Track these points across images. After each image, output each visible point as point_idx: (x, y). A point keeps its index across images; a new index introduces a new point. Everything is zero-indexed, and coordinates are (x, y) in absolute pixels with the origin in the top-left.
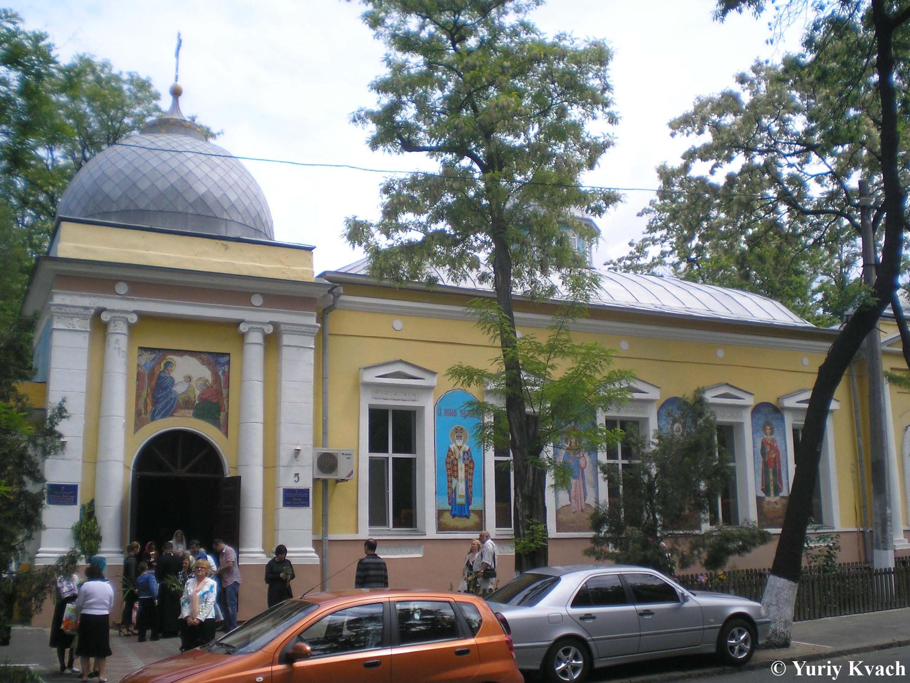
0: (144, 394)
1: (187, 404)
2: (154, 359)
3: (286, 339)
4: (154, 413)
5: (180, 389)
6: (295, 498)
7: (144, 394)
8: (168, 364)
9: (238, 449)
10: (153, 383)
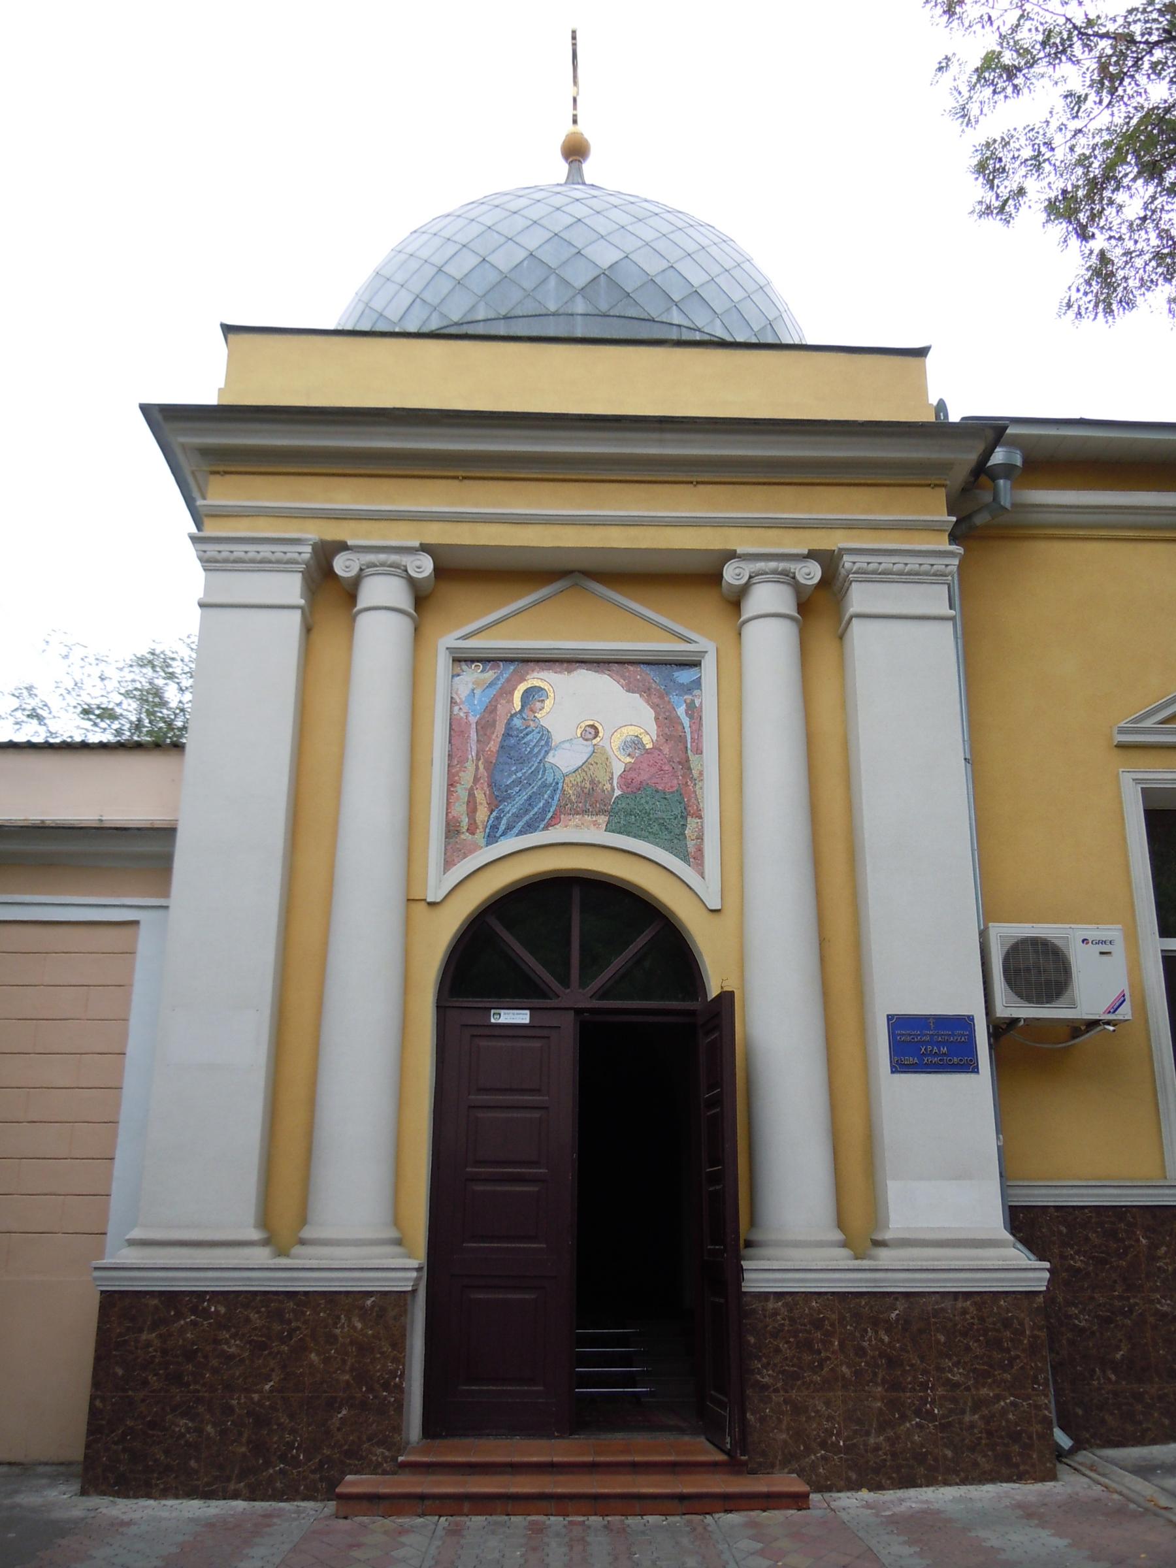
0: (467, 778)
1: (590, 800)
2: (491, 685)
3: (860, 598)
4: (495, 827)
5: (566, 758)
6: (927, 1045)
7: (467, 778)
8: (533, 695)
9: (732, 909)
10: (493, 746)
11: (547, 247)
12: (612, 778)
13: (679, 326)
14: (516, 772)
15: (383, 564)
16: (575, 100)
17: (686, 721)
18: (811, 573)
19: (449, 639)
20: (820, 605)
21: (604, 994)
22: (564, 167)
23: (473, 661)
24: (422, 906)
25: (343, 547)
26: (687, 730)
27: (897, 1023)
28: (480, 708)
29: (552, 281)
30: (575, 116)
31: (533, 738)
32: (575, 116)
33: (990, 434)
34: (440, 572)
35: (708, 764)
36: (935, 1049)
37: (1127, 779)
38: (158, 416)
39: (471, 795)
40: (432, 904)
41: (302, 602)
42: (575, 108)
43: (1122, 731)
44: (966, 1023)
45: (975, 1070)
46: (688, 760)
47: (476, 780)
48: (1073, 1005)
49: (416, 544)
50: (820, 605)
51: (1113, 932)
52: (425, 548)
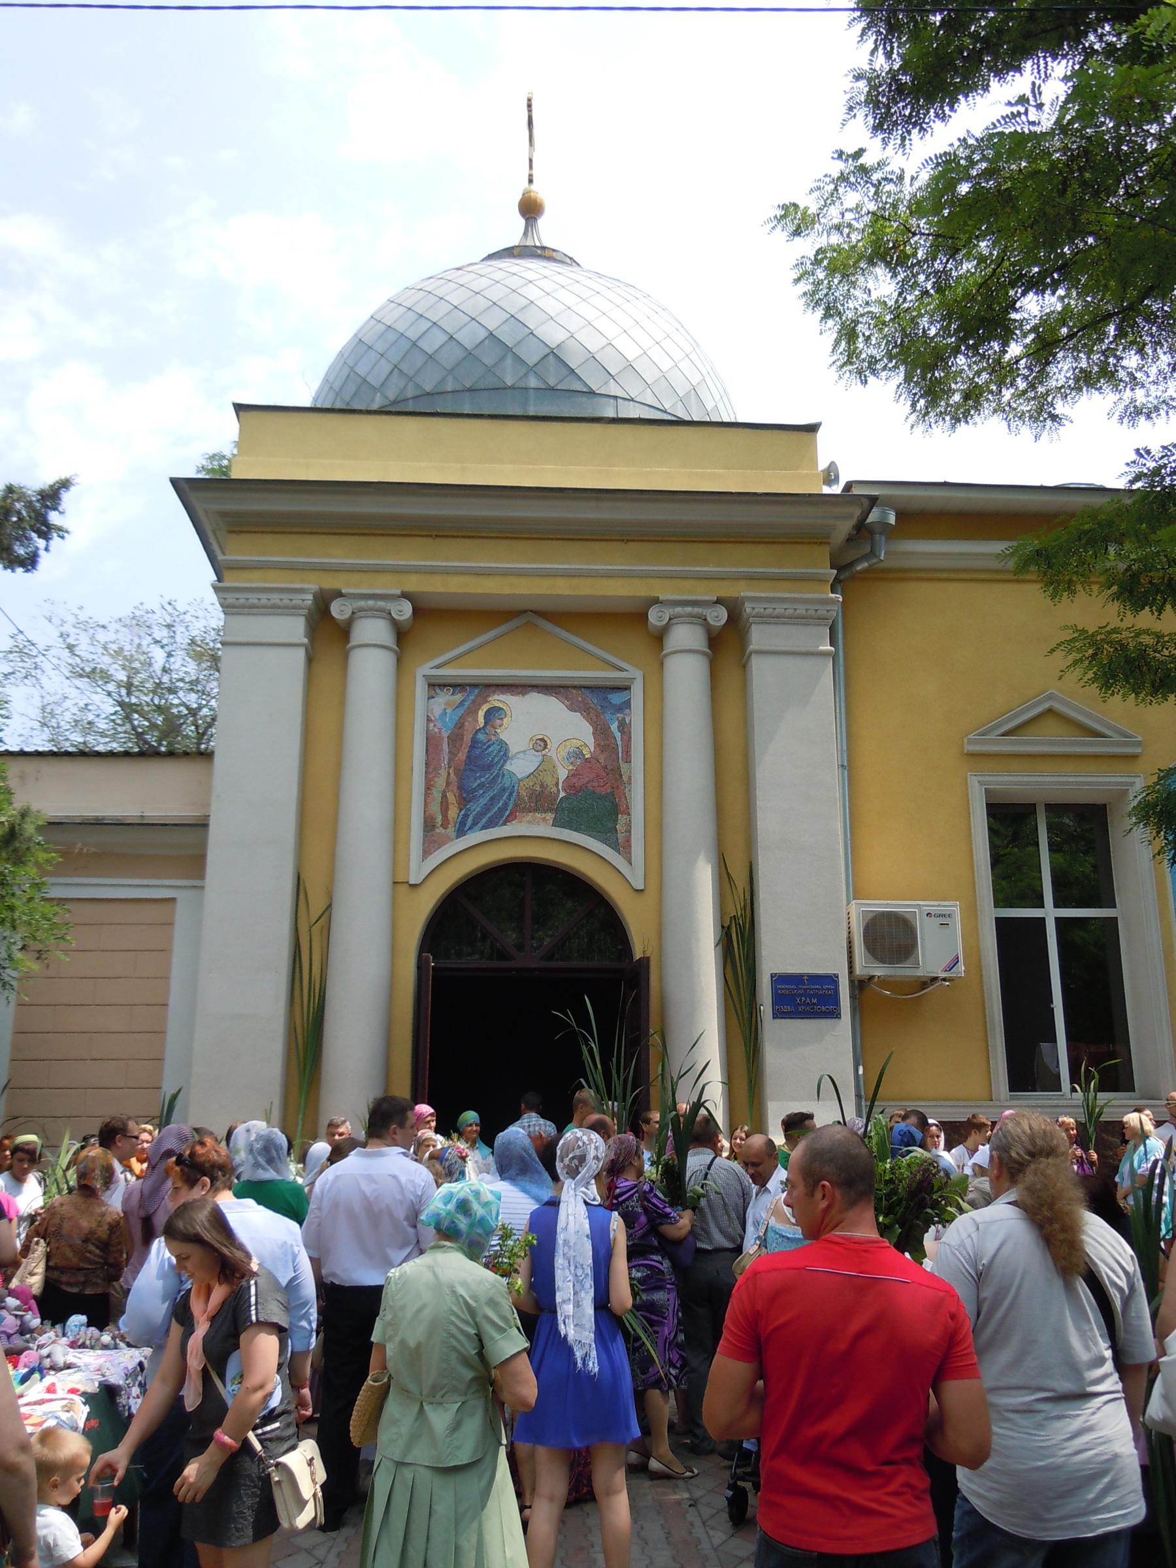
0: (440, 782)
1: (539, 800)
2: (461, 704)
3: (759, 637)
4: (463, 823)
5: (521, 766)
6: (807, 997)
7: (440, 782)
8: (492, 713)
10: (462, 756)
11: (504, 327)
12: (557, 784)
13: (616, 397)
14: (480, 777)
15: (371, 609)
16: (531, 160)
17: (618, 735)
18: (719, 617)
19: (425, 669)
20: (727, 644)
22: (522, 222)
23: (445, 686)
24: (405, 888)
25: (339, 594)
26: (619, 743)
27: (779, 980)
28: (451, 725)
29: (509, 361)
30: (531, 176)
31: (494, 749)
32: (531, 176)
34: (419, 612)
35: (637, 770)
36: (808, 1000)
38: (186, 487)
39: (444, 796)
40: (414, 886)
41: (306, 641)
42: (531, 167)
43: (970, 742)
44: (832, 980)
45: (837, 1015)
46: (619, 768)
47: (448, 784)
48: (916, 965)
49: (398, 592)
50: (727, 644)
51: (955, 908)
52: (405, 595)
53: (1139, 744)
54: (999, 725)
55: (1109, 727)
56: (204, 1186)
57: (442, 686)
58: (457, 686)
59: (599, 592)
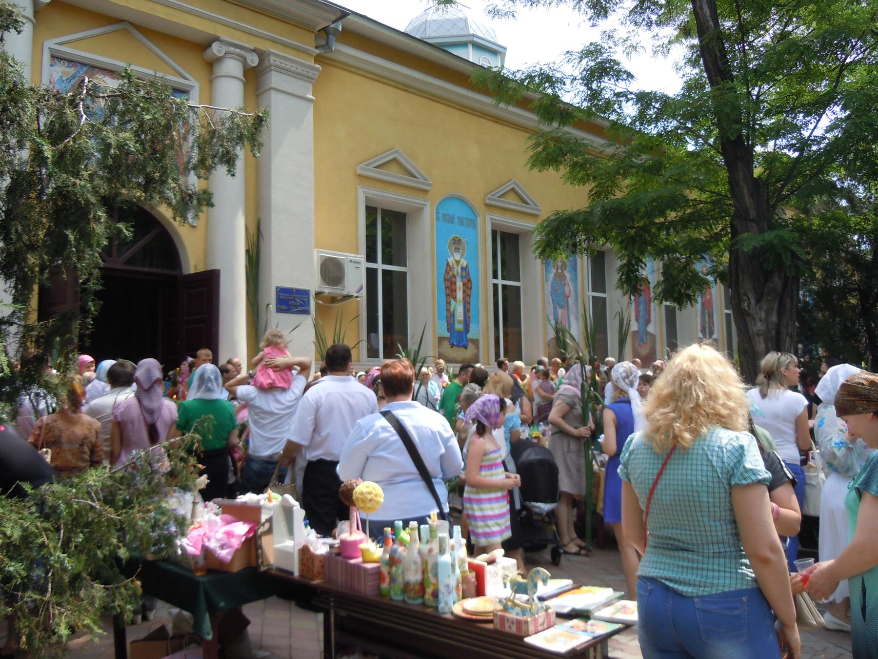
3: (275, 79)
19: (51, 43)
21: (129, 262)
27: (281, 291)
33: (339, 14)
37: (361, 191)
53: (430, 185)
54: (374, 162)
55: (419, 174)
56: (105, 467)
57: (61, 59)
58: (71, 61)
59: (183, 22)
